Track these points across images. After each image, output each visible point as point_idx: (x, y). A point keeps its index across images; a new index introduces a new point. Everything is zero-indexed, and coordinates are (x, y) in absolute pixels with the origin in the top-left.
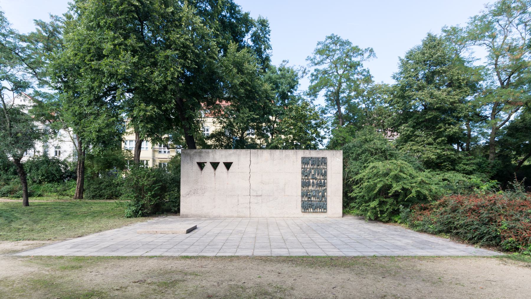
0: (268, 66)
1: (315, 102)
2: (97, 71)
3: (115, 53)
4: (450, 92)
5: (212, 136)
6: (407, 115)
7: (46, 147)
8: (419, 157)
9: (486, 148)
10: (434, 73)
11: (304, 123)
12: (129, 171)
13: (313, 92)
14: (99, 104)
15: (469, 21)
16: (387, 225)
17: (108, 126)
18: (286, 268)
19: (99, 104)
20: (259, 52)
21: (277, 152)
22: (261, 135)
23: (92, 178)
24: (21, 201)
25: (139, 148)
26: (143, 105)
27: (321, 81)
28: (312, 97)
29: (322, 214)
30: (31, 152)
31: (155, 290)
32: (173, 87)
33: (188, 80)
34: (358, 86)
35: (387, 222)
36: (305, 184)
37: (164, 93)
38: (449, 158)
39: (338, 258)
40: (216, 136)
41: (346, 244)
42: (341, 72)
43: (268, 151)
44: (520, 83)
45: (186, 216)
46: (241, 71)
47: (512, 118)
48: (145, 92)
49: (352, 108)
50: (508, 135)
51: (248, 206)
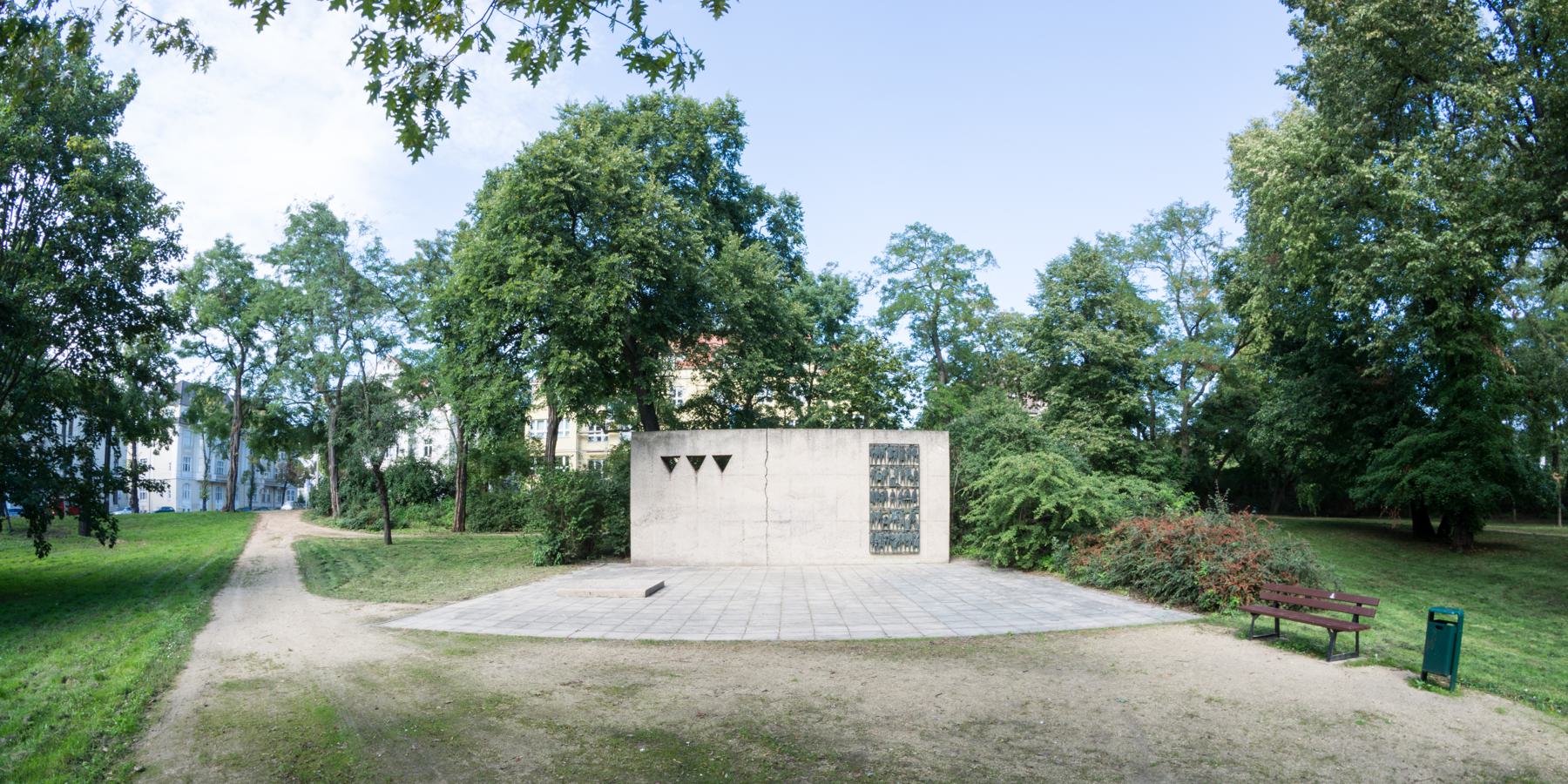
0: (800, 272)
1: (893, 339)
2: (496, 303)
3: (526, 270)
4: (1120, 337)
5: (690, 405)
6: (1058, 372)
7: (412, 441)
8: (1082, 449)
9: (1182, 433)
10: (1094, 303)
11: (873, 378)
12: (537, 478)
13: (888, 319)
14: (493, 359)
15: (1132, 229)
16: (1030, 576)
17: (506, 396)
18: (845, 663)
19: (493, 359)
20: (783, 248)
21: (821, 433)
22: (786, 400)
23: (478, 493)
24: (381, 535)
25: (554, 433)
26: (565, 353)
27: (901, 301)
28: (886, 330)
30: (392, 451)
31: (600, 700)
32: (621, 317)
33: (646, 301)
34: (971, 312)
35: (1030, 570)
36: (876, 498)
37: (603, 327)
38: (1127, 452)
39: (944, 641)
40: (698, 404)
41: (958, 614)
42: (937, 286)
43: (803, 431)
44: (1211, 336)
45: (643, 564)
46: (747, 281)
47: (1206, 391)
48: (570, 330)
49: (962, 352)
50: (1205, 417)
51: (763, 542)
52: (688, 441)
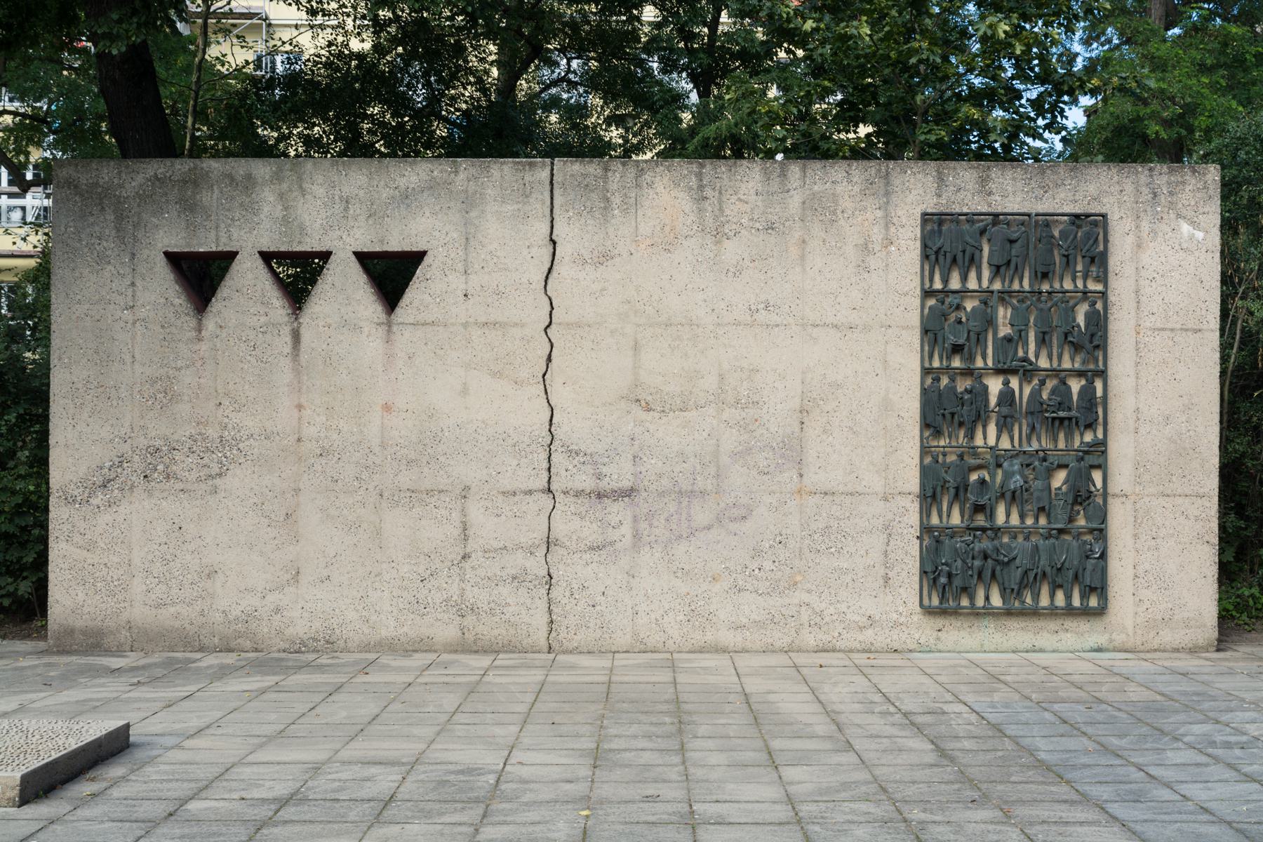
29: (1070, 623)
36: (944, 411)
45: (93, 642)
52: (268, 198)
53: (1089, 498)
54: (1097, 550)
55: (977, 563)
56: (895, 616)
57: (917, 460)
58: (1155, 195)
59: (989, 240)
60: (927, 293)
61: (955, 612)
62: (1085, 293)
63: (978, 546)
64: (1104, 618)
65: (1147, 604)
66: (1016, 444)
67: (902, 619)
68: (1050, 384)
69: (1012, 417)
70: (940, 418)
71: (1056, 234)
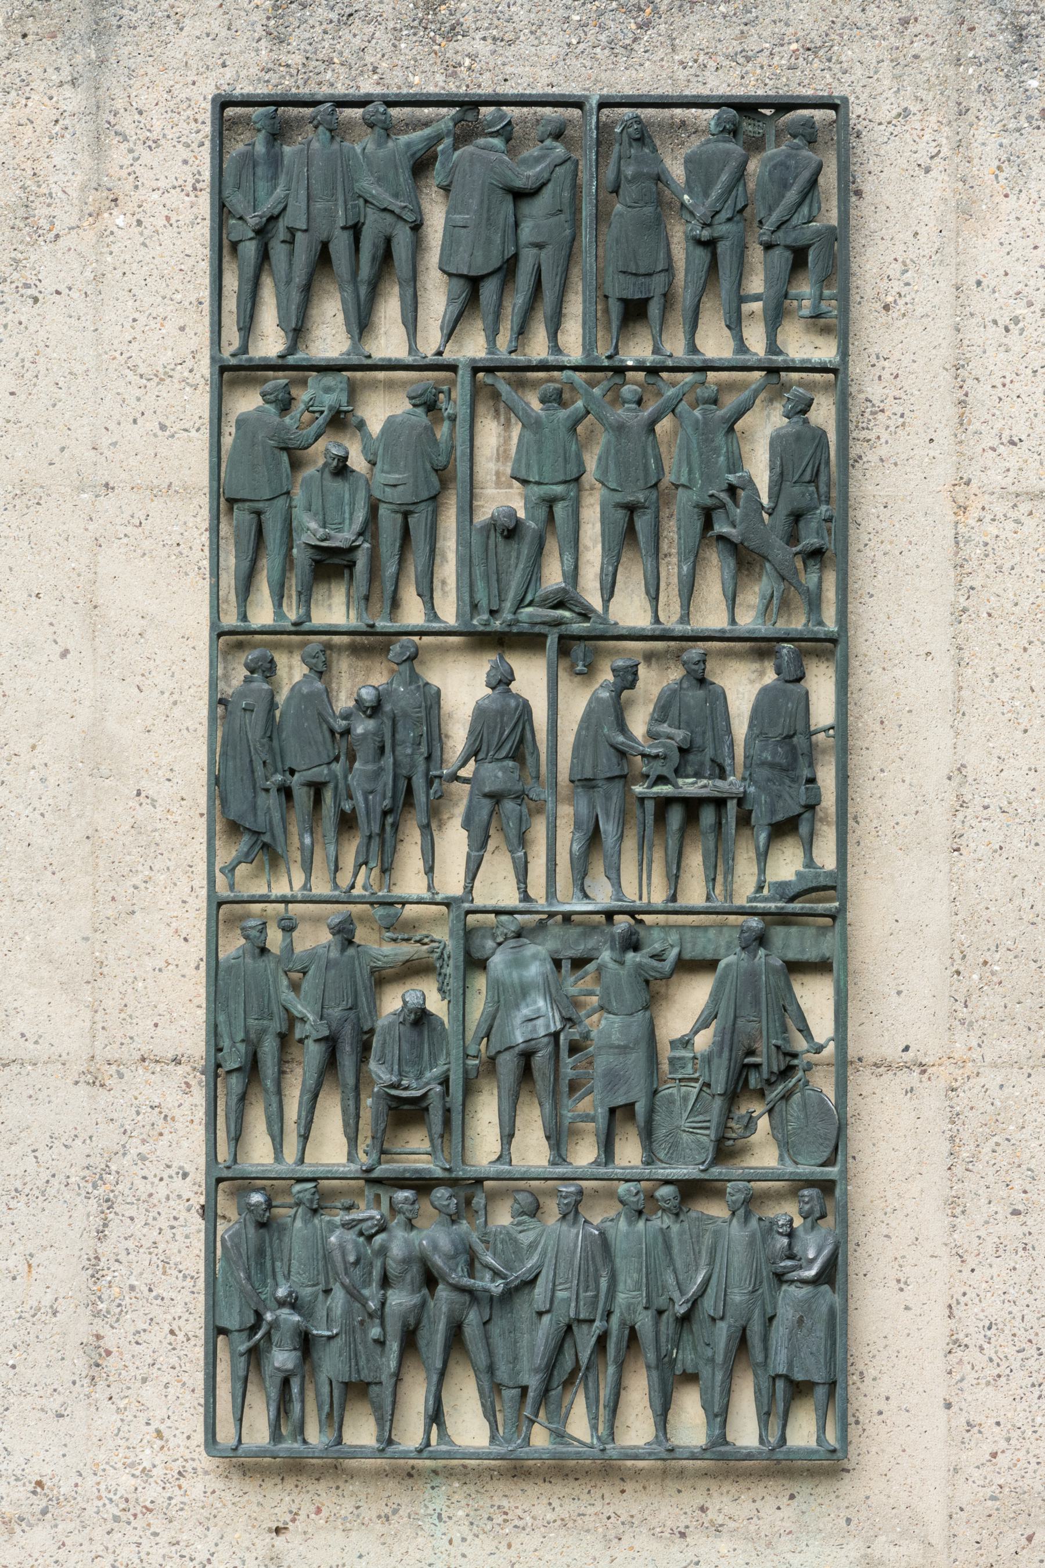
29: (728, 1503)
36: (296, 777)
53: (787, 1072)
54: (813, 1250)
55: (400, 1299)
56: (126, 1482)
57: (198, 948)
58: (1020, 35)
59: (446, 189)
60: (231, 373)
61: (333, 1466)
62: (773, 371)
63: (398, 1243)
64: (846, 1484)
65: (993, 1438)
66: (537, 887)
67: (152, 1493)
68: (654, 682)
69: (520, 797)
70: (272, 801)
71: (676, 170)
